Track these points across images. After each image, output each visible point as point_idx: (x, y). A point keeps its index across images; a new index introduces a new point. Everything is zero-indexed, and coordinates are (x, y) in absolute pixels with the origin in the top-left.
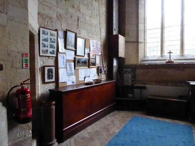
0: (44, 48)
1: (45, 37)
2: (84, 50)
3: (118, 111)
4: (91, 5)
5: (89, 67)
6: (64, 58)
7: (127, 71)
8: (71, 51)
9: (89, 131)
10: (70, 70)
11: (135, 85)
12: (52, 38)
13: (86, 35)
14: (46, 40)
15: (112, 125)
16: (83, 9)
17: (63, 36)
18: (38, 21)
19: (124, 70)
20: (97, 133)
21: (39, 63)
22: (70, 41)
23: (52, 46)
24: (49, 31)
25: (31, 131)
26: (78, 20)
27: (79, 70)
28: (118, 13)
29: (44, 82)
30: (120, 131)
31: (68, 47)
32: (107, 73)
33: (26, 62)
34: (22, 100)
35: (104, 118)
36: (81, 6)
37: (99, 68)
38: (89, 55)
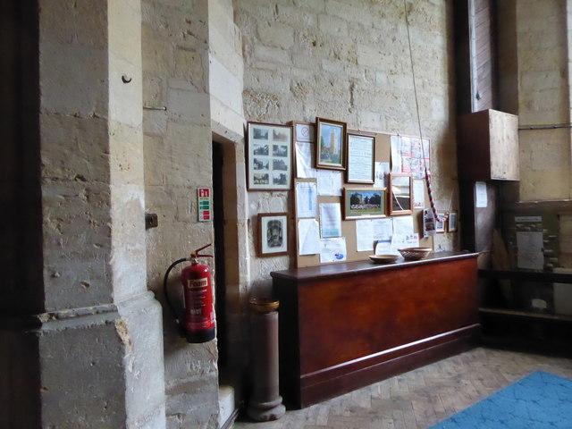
0: (257, 172)
1: (261, 143)
2: (371, 168)
3: (489, 351)
4: (394, 40)
5: (388, 214)
6: (310, 191)
7: (527, 224)
8: (331, 173)
9: (375, 394)
10: (329, 223)
11: (558, 270)
12: (279, 144)
13: (377, 125)
14: (262, 151)
15: (450, 387)
16: (366, 55)
17: (308, 137)
18: (245, 110)
19: (517, 219)
20: (398, 402)
21: (247, 207)
22: (329, 146)
23: (278, 165)
24: (270, 129)
25: (216, 365)
26: (352, 88)
27: (357, 222)
28: (488, 44)
29: (258, 253)
30: (469, 409)
31: (321, 162)
32: (456, 232)
33: (205, 208)
34: (191, 290)
35: (435, 364)
36: (360, 49)
37: (425, 217)
38: (387, 180)
